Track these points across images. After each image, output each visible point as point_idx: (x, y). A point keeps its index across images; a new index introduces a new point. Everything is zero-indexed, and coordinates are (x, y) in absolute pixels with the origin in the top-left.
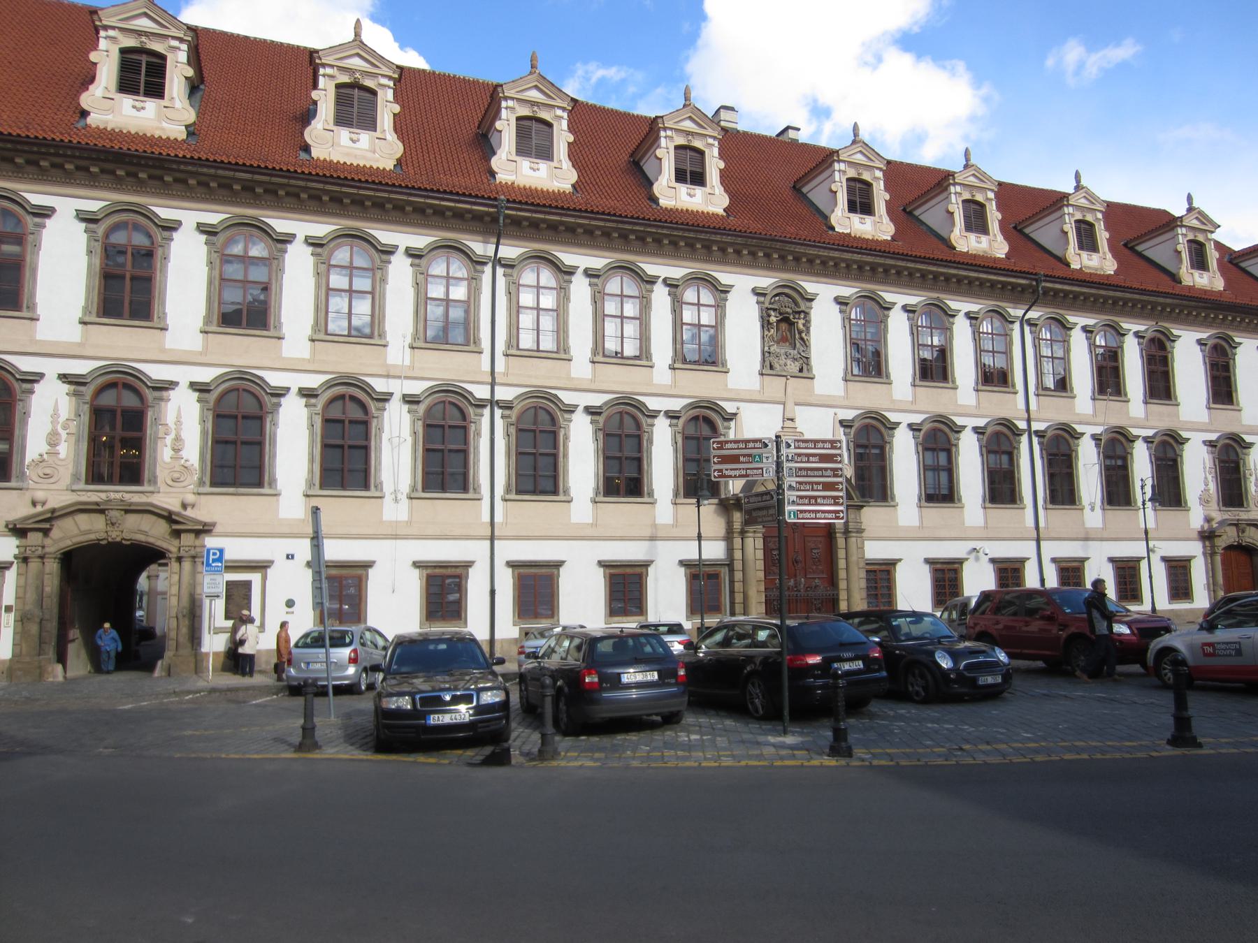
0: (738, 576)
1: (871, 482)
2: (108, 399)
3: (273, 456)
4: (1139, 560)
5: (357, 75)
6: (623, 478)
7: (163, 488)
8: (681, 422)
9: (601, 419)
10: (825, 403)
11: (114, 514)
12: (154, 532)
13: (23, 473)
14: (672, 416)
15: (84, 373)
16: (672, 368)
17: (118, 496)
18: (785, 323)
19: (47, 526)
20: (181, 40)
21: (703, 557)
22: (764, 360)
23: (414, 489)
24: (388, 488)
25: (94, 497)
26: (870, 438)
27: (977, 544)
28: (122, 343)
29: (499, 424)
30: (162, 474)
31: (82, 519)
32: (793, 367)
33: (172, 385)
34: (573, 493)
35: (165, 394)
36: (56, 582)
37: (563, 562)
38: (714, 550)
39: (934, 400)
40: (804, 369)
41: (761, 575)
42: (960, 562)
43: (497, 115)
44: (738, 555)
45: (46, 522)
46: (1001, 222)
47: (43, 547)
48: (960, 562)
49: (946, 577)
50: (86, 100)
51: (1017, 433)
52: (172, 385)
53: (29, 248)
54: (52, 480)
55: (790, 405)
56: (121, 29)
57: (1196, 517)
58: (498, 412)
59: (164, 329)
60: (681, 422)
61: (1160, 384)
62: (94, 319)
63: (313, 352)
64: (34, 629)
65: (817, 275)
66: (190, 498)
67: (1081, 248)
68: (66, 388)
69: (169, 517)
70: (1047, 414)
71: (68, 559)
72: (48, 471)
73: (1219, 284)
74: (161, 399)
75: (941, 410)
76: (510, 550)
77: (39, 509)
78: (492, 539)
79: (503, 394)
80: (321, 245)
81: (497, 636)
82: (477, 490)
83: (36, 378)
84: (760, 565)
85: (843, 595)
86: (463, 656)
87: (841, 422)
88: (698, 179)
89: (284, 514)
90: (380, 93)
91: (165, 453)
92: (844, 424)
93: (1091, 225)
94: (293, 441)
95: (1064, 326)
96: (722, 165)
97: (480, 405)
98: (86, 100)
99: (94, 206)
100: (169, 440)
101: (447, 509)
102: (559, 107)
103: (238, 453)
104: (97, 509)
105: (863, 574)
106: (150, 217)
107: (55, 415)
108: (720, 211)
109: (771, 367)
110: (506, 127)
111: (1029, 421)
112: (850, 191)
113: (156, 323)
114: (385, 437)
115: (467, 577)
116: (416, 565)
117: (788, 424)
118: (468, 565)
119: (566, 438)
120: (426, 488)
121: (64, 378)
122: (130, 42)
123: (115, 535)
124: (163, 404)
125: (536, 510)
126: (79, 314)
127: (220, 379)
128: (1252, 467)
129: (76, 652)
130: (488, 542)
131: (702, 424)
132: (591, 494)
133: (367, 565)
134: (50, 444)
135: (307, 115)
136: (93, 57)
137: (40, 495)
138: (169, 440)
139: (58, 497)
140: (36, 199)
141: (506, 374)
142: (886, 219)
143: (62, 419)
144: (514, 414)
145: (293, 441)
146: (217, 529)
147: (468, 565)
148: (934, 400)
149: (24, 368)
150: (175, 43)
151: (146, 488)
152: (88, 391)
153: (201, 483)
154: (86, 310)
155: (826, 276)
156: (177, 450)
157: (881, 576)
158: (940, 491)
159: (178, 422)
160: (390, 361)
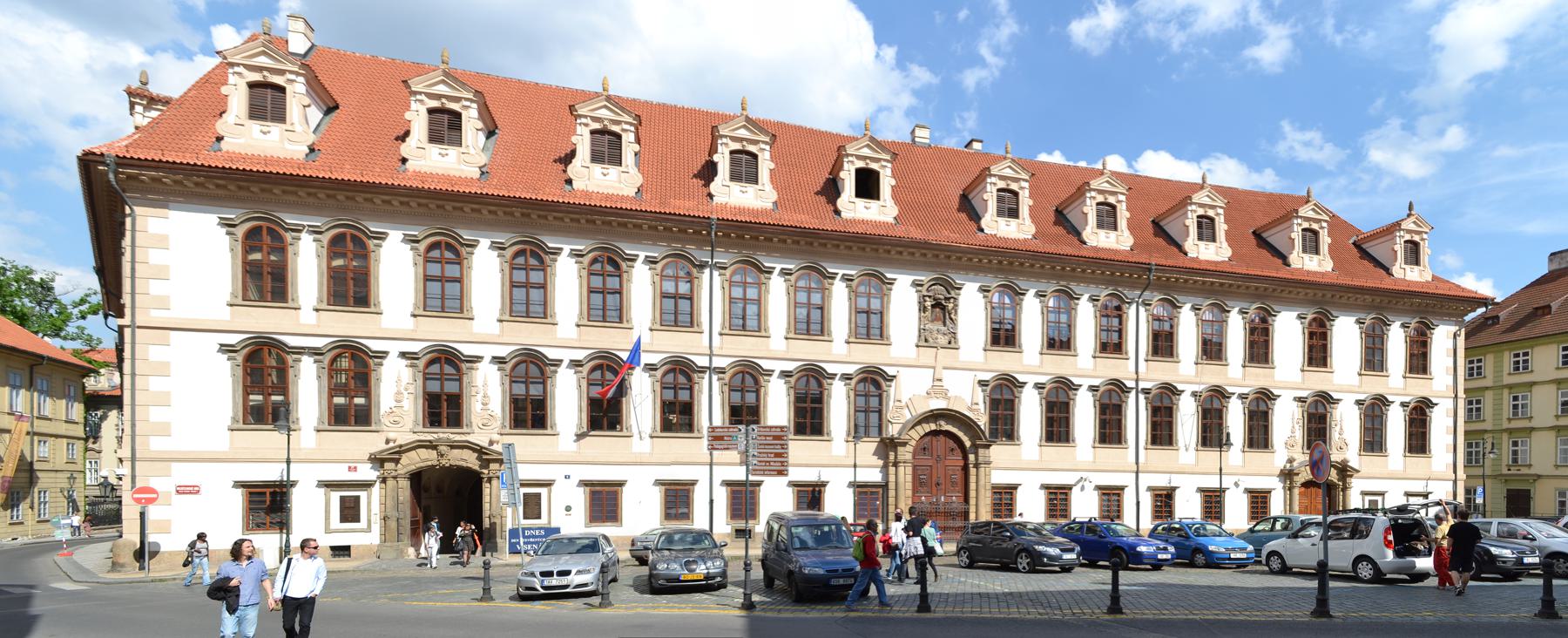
0: (892, 493)
1: (1004, 424)
3: (553, 408)
8: (853, 382)
9: (793, 380)
11: (443, 449)
12: (470, 460)
14: (846, 377)
18: (940, 308)
20: (297, 74)
25: (429, 437)
26: (1003, 396)
27: (1084, 475)
29: (716, 385)
31: (422, 451)
32: (943, 340)
33: (478, 359)
34: (833, 434)
38: (874, 476)
39: (1058, 365)
40: (952, 343)
41: (910, 493)
42: (1070, 488)
43: (841, 168)
44: (892, 478)
46: (1227, 233)
48: (1070, 488)
49: (1058, 497)
50: (222, 126)
51: (1128, 390)
52: (478, 359)
53: (290, 255)
56: (245, 66)
58: (715, 377)
60: (853, 382)
61: (1259, 350)
63: (580, 334)
65: (776, 250)
66: (496, 437)
67: (1304, 251)
68: (405, 362)
69: (480, 451)
70: (1155, 373)
71: (416, 478)
73: (1328, 265)
79: (719, 362)
83: (383, 355)
84: (909, 485)
85: (972, 509)
86: (829, 533)
88: (1014, 213)
90: (624, 136)
92: (983, 383)
93: (1212, 220)
94: (567, 398)
95: (1072, 298)
96: (893, 182)
97: (702, 370)
98: (222, 126)
104: (431, 446)
105: (989, 494)
107: (399, 380)
108: (891, 220)
110: (990, 196)
111: (1137, 381)
112: (1000, 200)
113: (465, 314)
116: (659, 483)
118: (693, 483)
121: (403, 355)
129: (432, 541)
133: (621, 484)
136: (224, 90)
137: (392, 435)
138: (479, 397)
139: (404, 438)
140: (374, 228)
142: (1225, 245)
143: (404, 383)
144: (727, 377)
145: (567, 398)
147: (693, 483)
148: (1058, 365)
149: (374, 348)
150: (292, 77)
151: (465, 430)
152: (421, 363)
157: (1005, 496)
159: (485, 385)
160: (1080, 365)
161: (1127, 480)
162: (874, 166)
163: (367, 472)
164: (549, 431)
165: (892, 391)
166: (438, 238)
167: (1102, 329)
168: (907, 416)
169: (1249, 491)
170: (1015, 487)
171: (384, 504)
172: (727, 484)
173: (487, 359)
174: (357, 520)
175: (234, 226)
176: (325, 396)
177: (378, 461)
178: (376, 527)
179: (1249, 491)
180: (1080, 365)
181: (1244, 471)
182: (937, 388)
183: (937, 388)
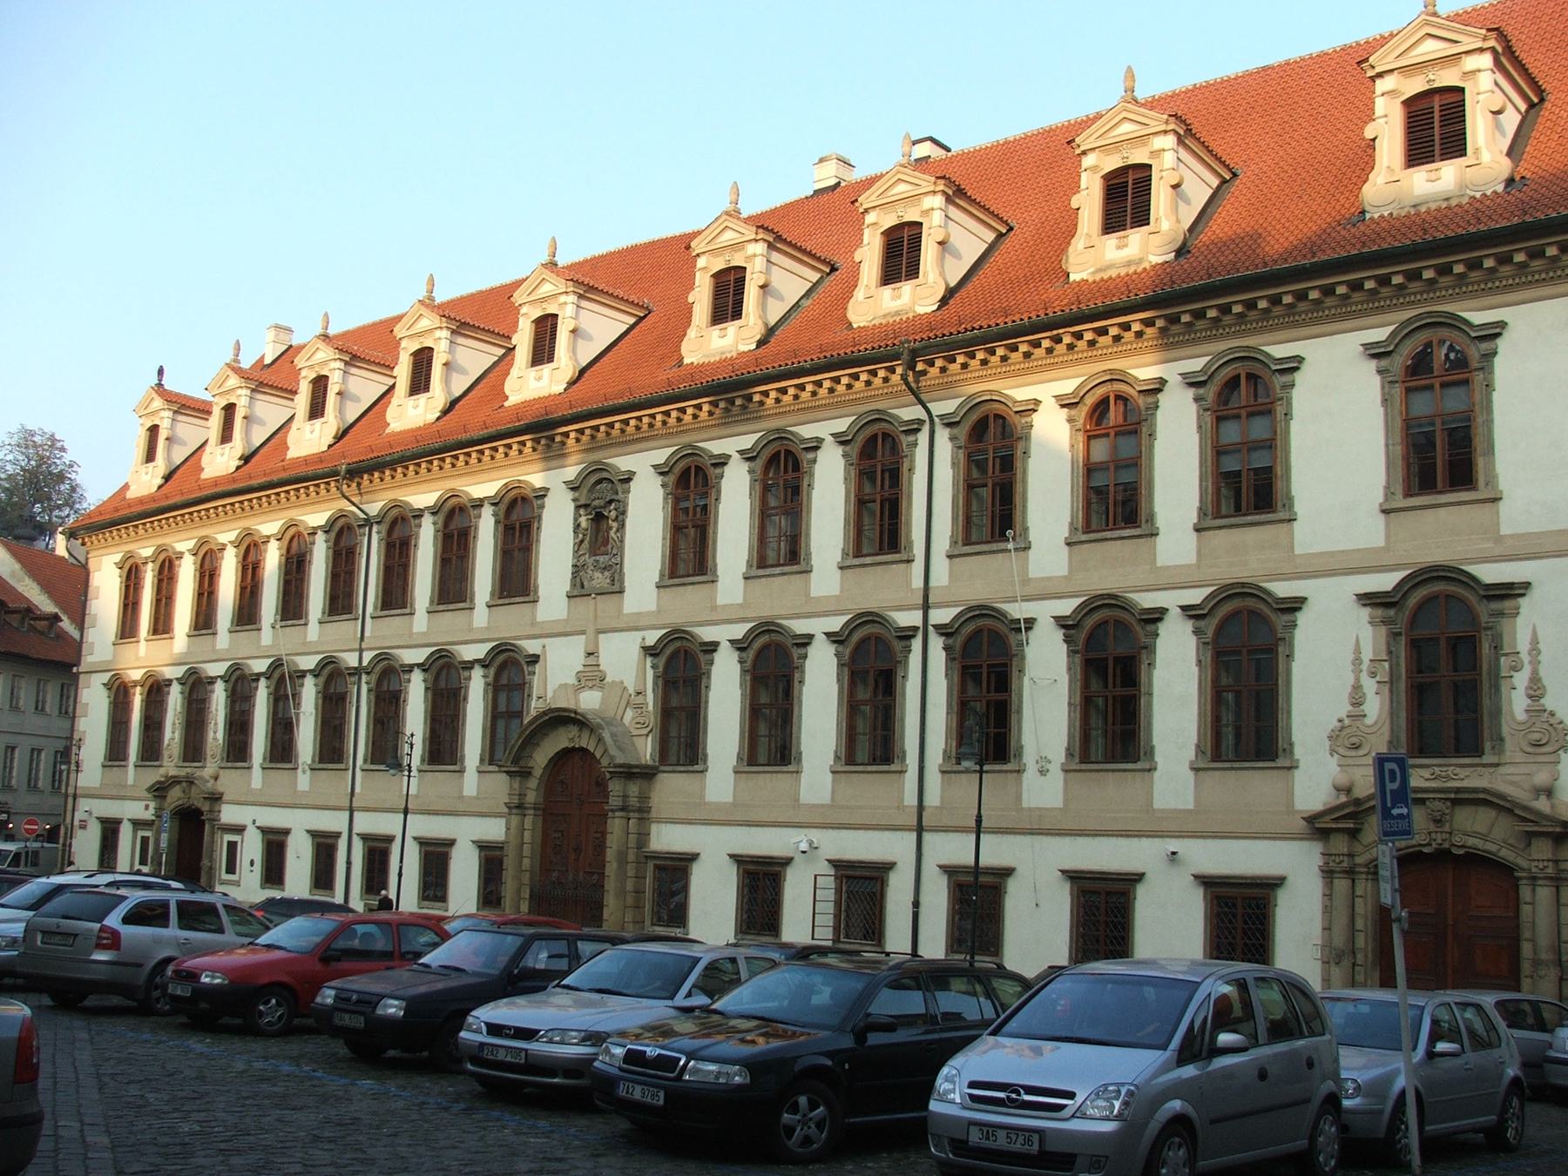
1: (682, 736)
4: (338, 835)
15: (1389, 588)
21: (983, 862)
22: (574, 578)
24: (1029, 758)
35: (1508, 604)
37: (731, 856)
40: (616, 589)
47: (1351, 855)
54: (1361, 752)
57: (1317, 774)
59: (1496, 500)
61: (1248, 486)
72: (1354, 740)
74: (1501, 614)
75: (871, 604)
78: (920, 830)
80: (1388, 354)
91: (211, 734)
99: (1380, 334)
118: (888, 867)
120: (1217, 756)
124: (1505, 622)
126: (1378, 496)
128: (1523, 645)
130: (347, 814)
131: (510, 668)
134: (1353, 704)
135: (1067, 227)
138: (1521, 679)
140: (1279, 351)
146: (225, 798)
147: (888, 867)
154: (1389, 492)
155: (1295, 325)
158: (770, 740)
160: (1034, 571)
161: (893, 847)
164: (1280, 762)
165: (536, 681)
166: (1422, 337)
167: (1216, 452)
169: (1208, 882)
170: (693, 857)
172: (949, 870)
175: (1388, 354)
179: (1208, 882)
180: (1034, 571)
181: (1178, 829)
183: (592, 675)
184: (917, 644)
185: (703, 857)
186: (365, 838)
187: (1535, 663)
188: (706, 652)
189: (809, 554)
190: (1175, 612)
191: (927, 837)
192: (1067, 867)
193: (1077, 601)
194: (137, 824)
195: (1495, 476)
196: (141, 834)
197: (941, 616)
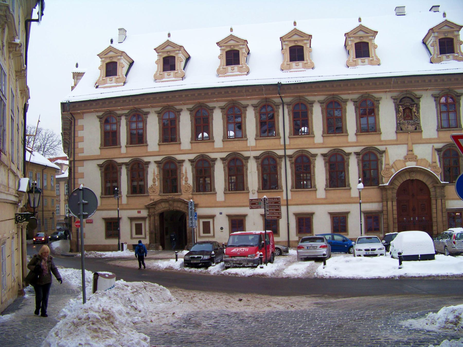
2: (168, 167)
5: (232, 47)
6: (337, 179)
7: (183, 193)
10: (428, 141)
13: (148, 191)
16: (396, 132)
17: (171, 196)
19: (154, 206)
23: (259, 189)
24: (250, 189)
28: (170, 150)
30: (183, 190)
32: (411, 128)
36: (158, 222)
40: (418, 129)
45: (155, 204)
55: (410, 143)
56: (354, 37)
61: (138, 138)
62: (359, 134)
64: (154, 236)
71: (162, 215)
76: (294, 209)
77: (152, 202)
81: (291, 239)
82: (281, 188)
87: (436, 149)
89: (318, 196)
91: (183, 182)
97: (280, 157)
100: (184, 178)
101: (338, 193)
102: (370, 36)
103: (203, 181)
104: (166, 201)
106: (207, 106)
107: (154, 173)
109: (401, 129)
114: (248, 172)
115: (348, 217)
117: (410, 153)
119: (314, 167)
122: (357, 41)
123: (171, 208)
125: (302, 195)
126: (157, 142)
127: (261, 155)
128: (184, 172)
132: (324, 187)
137: (152, 197)
138: (184, 178)
140: (146, 110)
141: (289, 145)
146: (200, 205)
153: (193, 191)
156: (186, 181)
159: (186, 172)
162: (300, 44)
163: (144, 213)
165: (383, 159)
168: (394, 172)
171: (150, 227)
173: (319, 155)
174: (141, 234)
176: (129, 183)
177: (148, 207)
178: (148, 237)
182: (410, 156)
183: (410, 156)
184: (283, 160)
185: (351, 212)
186: (296, 215)
187: (186, 175)
188: (212, 161)
189: (180, 139)
190: (252, 157)
191: (289, 207)
192: (105, 217)
193: (130, 159)
194: (132, 219)
195: (461, 125)
196: (134, 223)
197: (289, 152)
